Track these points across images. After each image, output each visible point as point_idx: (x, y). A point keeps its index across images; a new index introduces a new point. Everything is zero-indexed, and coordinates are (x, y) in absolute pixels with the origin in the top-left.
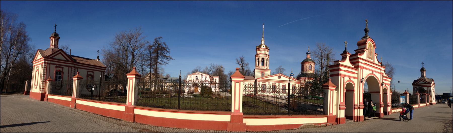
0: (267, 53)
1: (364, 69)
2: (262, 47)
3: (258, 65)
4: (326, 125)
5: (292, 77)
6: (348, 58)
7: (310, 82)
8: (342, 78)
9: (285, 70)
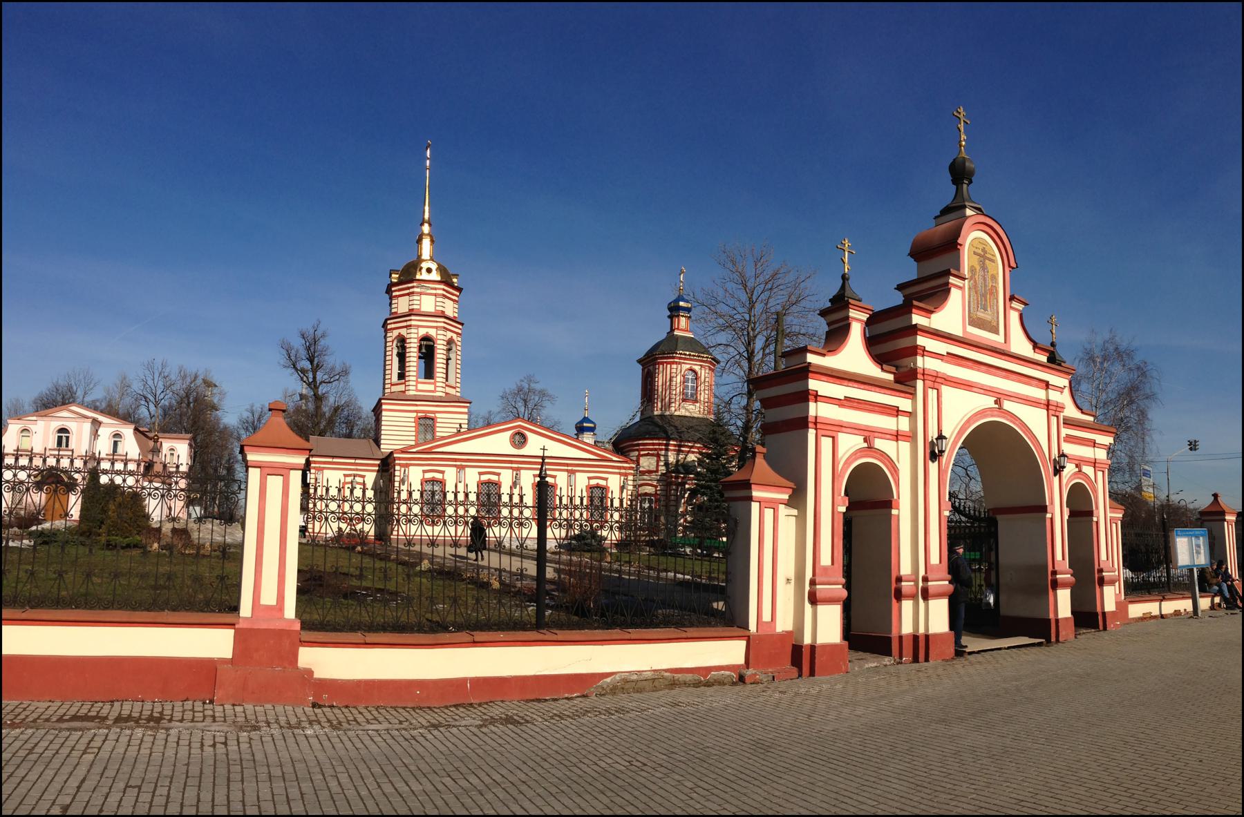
0: (450, 309)
1: (946, 390)
2: (423, 275)
3: (402, 376)
4: (742, 679)
5: (588, 438)
6: (856, 331)
7: (687, 468)
8: (826, 443)
9: (551, 398)
